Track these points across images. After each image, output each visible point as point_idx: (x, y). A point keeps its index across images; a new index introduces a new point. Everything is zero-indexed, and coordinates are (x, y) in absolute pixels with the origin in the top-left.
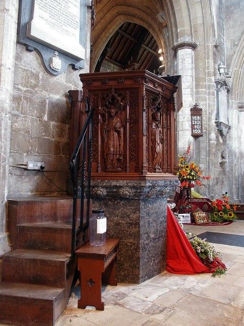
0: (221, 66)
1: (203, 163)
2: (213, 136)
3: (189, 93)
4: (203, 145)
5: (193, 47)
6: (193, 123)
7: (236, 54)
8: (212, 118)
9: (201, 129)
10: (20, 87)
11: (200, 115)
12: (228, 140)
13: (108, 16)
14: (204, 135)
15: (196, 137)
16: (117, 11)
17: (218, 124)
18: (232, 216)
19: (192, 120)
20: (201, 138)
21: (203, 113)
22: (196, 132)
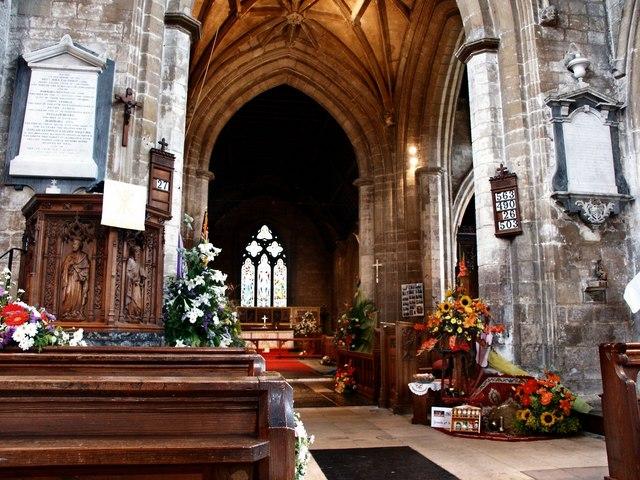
0: (572, 62)
1: (526, 294)
2: (549, 229)
3: (486, 146)
4: (525, 254)
5: (491, 45)
6: (498, 209)
7: (628, 14)
8: (544, 188)
9: (519, 219)
10: (7, 232)
11: (515, 188)
12: (632, 231)
13: (434, 27)
14: (527, 231)
15: (508, 237)
16: (442, 13)
17: (563, 200)
18: (542, 418)
19: (494, 202)
20: (519, 240)
21: (522, 183)
22: (505, 226)
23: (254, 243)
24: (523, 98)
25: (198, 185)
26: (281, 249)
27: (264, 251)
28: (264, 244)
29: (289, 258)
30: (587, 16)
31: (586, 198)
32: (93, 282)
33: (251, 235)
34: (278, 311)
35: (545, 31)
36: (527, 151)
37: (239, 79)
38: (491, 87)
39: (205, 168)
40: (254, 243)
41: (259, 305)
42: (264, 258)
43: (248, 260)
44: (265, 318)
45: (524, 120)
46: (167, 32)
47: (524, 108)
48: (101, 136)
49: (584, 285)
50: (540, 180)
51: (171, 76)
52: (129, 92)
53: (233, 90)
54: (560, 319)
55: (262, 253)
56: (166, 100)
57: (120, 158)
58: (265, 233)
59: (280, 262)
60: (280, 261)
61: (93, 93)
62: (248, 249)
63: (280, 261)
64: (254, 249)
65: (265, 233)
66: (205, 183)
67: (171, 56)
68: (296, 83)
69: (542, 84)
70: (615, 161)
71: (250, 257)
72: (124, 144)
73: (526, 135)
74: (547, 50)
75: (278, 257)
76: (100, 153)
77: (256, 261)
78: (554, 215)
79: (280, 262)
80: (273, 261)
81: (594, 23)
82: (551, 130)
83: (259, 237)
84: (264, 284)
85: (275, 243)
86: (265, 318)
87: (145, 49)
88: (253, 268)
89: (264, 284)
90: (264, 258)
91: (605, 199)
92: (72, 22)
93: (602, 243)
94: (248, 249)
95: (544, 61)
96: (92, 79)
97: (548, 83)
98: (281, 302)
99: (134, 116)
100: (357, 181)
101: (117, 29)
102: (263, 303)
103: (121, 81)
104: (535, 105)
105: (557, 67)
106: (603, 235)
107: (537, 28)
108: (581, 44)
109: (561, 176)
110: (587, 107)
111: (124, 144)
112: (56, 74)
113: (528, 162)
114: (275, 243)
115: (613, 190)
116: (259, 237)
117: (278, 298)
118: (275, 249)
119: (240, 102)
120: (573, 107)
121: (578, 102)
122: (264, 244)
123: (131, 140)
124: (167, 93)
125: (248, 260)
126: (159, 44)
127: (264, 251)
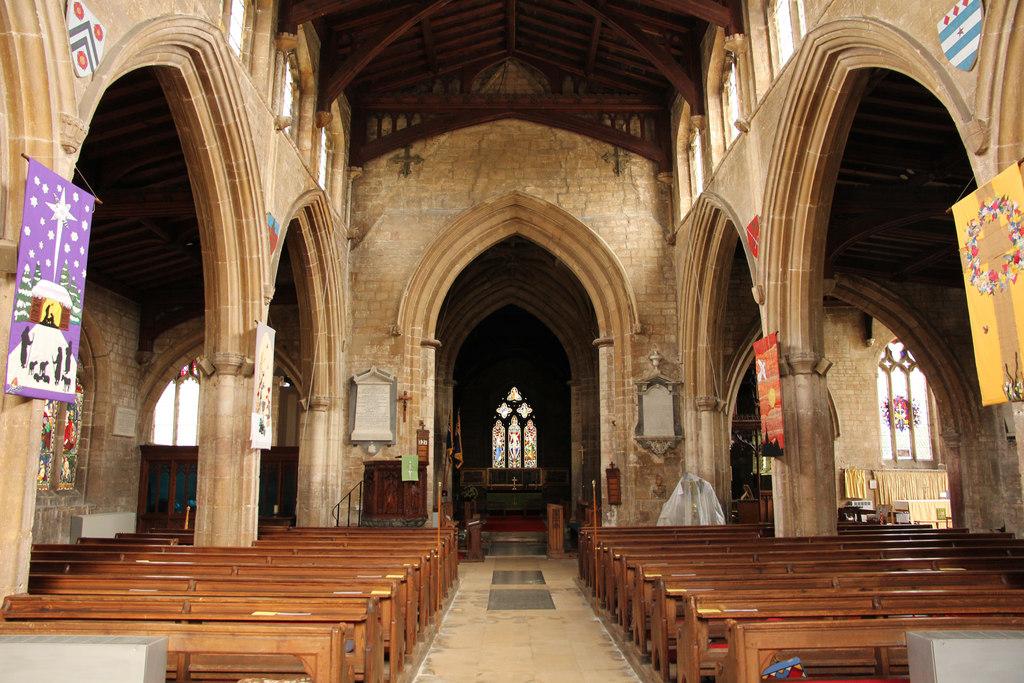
5: (610, 343)
23: (504, 405)
24: (623, 378)
25: (446, 391)
26: (530, 410)
27: (514, 413)
28: (514, 405)
29: (538, 418)
30: (665, 325)
31: (653, 440)
32: (288, 360)
33: (501, 398)
34: (530, 471)
35: (637, 337)
36: (624, 410)
37: (473, 307)
38: (609, 369)
39: (451, 377)
40: (504, 405)
41: (510, 466)
42: (515, 420)
43: (499, 422)
44: (514, 480)
45: (624, 392)
46: (422, 350)
47: (624, 385)
48: (393, 418)
49: (651, 488)
50: (630, 428)
51: (426, 376)
52: (405, 394)
53: (469, 316)
54: (637, 507)
55: (511, 415)
56: (424, 390)
57: (403, 429)
58: (515, 395)
59: (530, 423)
60: (530, 423)
61: (388, 395)
62: (498, 411)
63: (530, 423)
64: (504, 411)
65: (515, 395)
66: (450, 390)
67: (425, 364)
68: (520, 304)
69: (633, 370)
70: (674, 415)
71: (500, 418)
72: (405, 421)
73: (624, 401)
74: (638, 349)
75: (528, 418)
76: (393, 428)
77: (506, 422)
78: (636, 449)
79: (530, 423)
80: (523, 422)
81: (669, 328)
82: (636, 399)
83: (509, 398)
84: (515, 445)
85: (524, 405)
86: (514, 480)
87: (412, 366)
88: (503, 430)
89: (515, 445)
90: (515, 420)
91: (666, 440)
92: (375, 356)
93: (666, 465)
94: (498, 411)
95: (635, 357)
96: (387, 389)
97: (637, 370)
98: (532, 463)
99: (408, 405)
100: (596, 341)
101: (397, 359)
102: (515, 465)
103: (401, 388)
104: (629, 385)
105: (642, 360)
106: (666, 459)
107: (632, 336)
108: (660, 343)
109: (640, 428)
110: (658, 385)
111: (405, 421)
112: (369, 387)
113: (624, 417)
114: (524, 405)
115: (672, 434)
116: (509, 398)
117: (529, 458)
118: (525, 411)
119: (476, 322)
120: (649, 386)
121: (651, 384)
122: (514, 405)
123: (407, 417)
124: (424, 386)
125: (499, 422)
126: (418, 361)
127: (514, 413)
